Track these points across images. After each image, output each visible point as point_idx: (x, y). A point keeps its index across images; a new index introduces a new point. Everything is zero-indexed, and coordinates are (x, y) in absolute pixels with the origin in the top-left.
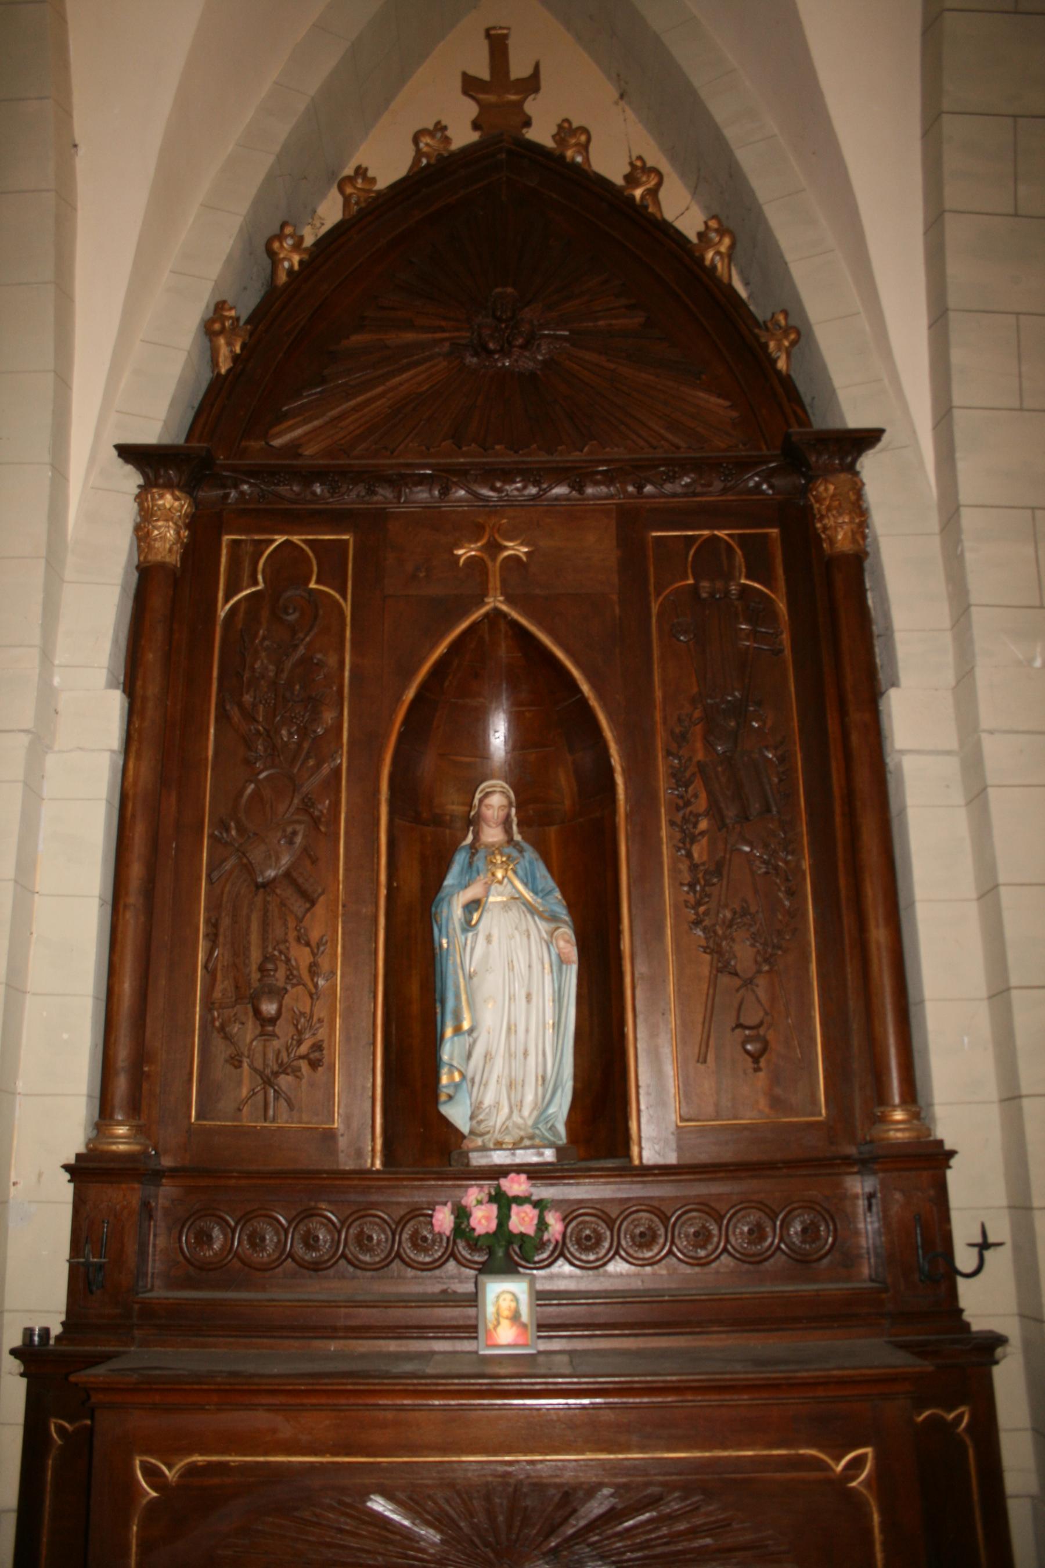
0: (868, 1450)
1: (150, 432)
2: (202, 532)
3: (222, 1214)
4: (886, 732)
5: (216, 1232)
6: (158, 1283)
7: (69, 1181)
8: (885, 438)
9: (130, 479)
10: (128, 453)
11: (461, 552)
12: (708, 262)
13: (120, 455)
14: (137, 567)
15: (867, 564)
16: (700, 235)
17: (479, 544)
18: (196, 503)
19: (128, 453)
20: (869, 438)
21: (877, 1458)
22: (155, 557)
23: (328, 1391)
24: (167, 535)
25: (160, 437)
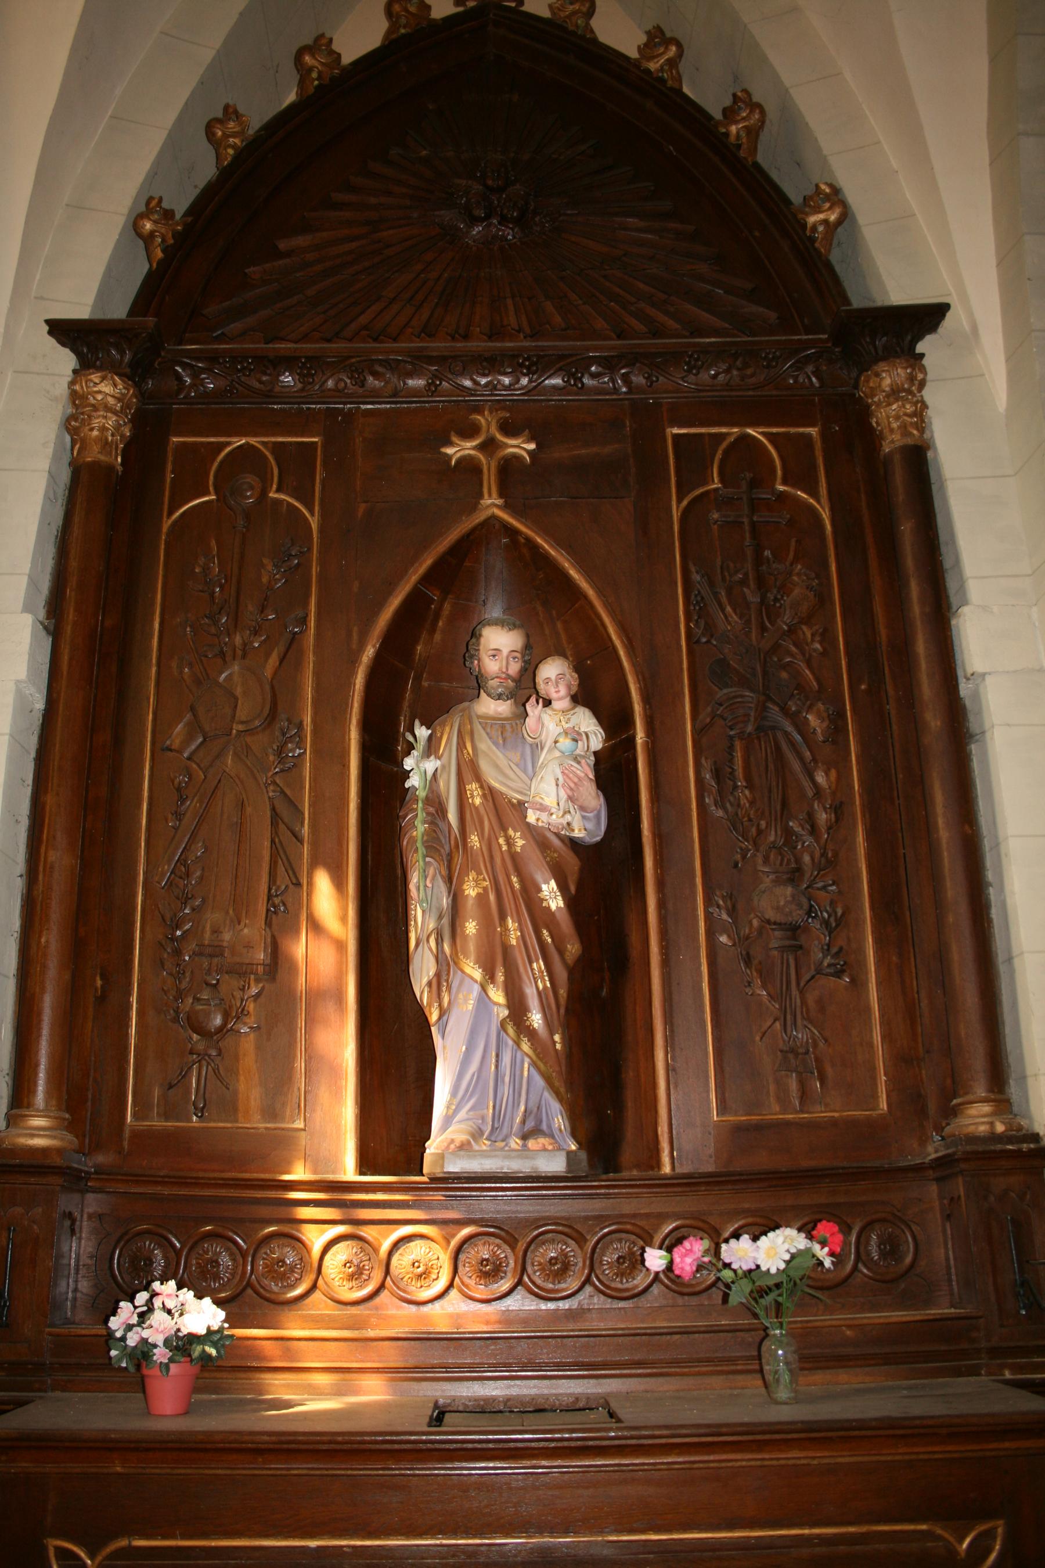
0: (1001, 1522)
1: (79, 306)
2: (148, 425)
3: (165, 1233)
4: (947, 563)
5: (225, 1260)
6: (81, 1315)
7: (768, 1270)
8: (949, 322)
9: (65, 360)
10: (62, 330)
11: (450, 451)
12: (732, 139)
13: (50, 333)
14: (70, 464)
15: (930, 454)
16: (725, 111)
17: (474, 444)
18: (143, 395)
19: (62, 330)
20: (929, 316)
21: (1011, 1539)
22: (95, 454)
23: (370, 1450)
24: (108, 426)
25: (93, 312)
